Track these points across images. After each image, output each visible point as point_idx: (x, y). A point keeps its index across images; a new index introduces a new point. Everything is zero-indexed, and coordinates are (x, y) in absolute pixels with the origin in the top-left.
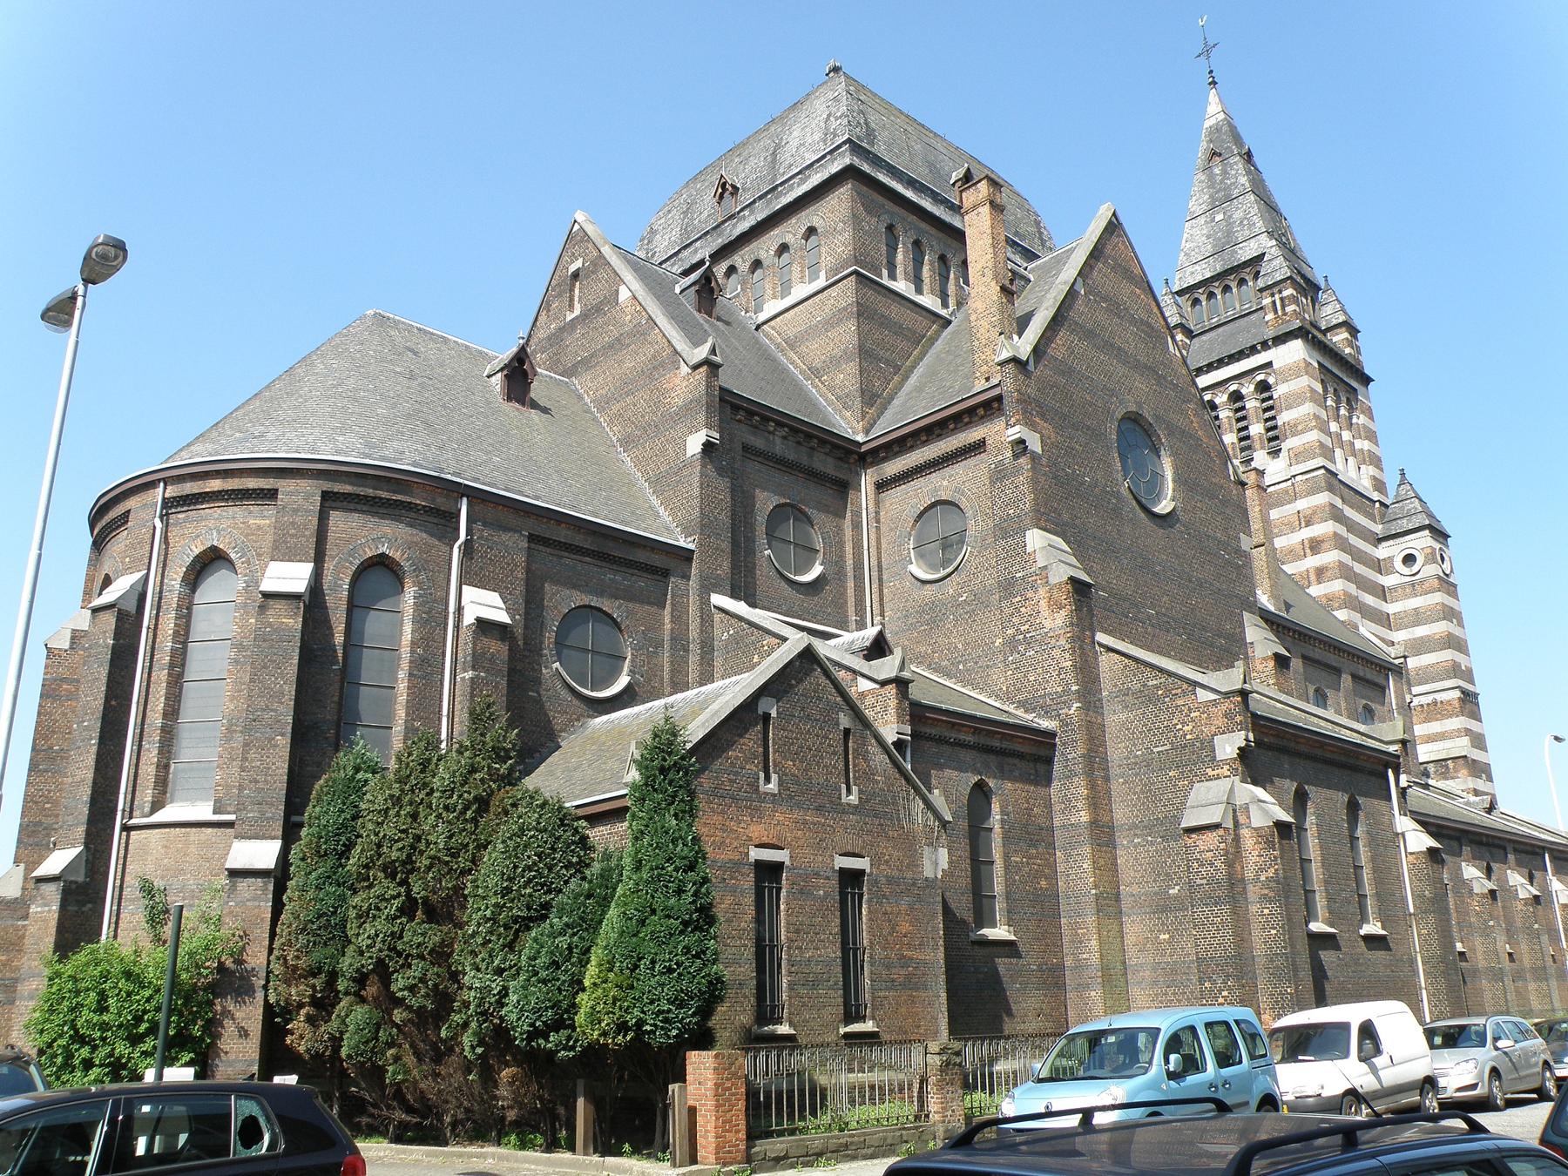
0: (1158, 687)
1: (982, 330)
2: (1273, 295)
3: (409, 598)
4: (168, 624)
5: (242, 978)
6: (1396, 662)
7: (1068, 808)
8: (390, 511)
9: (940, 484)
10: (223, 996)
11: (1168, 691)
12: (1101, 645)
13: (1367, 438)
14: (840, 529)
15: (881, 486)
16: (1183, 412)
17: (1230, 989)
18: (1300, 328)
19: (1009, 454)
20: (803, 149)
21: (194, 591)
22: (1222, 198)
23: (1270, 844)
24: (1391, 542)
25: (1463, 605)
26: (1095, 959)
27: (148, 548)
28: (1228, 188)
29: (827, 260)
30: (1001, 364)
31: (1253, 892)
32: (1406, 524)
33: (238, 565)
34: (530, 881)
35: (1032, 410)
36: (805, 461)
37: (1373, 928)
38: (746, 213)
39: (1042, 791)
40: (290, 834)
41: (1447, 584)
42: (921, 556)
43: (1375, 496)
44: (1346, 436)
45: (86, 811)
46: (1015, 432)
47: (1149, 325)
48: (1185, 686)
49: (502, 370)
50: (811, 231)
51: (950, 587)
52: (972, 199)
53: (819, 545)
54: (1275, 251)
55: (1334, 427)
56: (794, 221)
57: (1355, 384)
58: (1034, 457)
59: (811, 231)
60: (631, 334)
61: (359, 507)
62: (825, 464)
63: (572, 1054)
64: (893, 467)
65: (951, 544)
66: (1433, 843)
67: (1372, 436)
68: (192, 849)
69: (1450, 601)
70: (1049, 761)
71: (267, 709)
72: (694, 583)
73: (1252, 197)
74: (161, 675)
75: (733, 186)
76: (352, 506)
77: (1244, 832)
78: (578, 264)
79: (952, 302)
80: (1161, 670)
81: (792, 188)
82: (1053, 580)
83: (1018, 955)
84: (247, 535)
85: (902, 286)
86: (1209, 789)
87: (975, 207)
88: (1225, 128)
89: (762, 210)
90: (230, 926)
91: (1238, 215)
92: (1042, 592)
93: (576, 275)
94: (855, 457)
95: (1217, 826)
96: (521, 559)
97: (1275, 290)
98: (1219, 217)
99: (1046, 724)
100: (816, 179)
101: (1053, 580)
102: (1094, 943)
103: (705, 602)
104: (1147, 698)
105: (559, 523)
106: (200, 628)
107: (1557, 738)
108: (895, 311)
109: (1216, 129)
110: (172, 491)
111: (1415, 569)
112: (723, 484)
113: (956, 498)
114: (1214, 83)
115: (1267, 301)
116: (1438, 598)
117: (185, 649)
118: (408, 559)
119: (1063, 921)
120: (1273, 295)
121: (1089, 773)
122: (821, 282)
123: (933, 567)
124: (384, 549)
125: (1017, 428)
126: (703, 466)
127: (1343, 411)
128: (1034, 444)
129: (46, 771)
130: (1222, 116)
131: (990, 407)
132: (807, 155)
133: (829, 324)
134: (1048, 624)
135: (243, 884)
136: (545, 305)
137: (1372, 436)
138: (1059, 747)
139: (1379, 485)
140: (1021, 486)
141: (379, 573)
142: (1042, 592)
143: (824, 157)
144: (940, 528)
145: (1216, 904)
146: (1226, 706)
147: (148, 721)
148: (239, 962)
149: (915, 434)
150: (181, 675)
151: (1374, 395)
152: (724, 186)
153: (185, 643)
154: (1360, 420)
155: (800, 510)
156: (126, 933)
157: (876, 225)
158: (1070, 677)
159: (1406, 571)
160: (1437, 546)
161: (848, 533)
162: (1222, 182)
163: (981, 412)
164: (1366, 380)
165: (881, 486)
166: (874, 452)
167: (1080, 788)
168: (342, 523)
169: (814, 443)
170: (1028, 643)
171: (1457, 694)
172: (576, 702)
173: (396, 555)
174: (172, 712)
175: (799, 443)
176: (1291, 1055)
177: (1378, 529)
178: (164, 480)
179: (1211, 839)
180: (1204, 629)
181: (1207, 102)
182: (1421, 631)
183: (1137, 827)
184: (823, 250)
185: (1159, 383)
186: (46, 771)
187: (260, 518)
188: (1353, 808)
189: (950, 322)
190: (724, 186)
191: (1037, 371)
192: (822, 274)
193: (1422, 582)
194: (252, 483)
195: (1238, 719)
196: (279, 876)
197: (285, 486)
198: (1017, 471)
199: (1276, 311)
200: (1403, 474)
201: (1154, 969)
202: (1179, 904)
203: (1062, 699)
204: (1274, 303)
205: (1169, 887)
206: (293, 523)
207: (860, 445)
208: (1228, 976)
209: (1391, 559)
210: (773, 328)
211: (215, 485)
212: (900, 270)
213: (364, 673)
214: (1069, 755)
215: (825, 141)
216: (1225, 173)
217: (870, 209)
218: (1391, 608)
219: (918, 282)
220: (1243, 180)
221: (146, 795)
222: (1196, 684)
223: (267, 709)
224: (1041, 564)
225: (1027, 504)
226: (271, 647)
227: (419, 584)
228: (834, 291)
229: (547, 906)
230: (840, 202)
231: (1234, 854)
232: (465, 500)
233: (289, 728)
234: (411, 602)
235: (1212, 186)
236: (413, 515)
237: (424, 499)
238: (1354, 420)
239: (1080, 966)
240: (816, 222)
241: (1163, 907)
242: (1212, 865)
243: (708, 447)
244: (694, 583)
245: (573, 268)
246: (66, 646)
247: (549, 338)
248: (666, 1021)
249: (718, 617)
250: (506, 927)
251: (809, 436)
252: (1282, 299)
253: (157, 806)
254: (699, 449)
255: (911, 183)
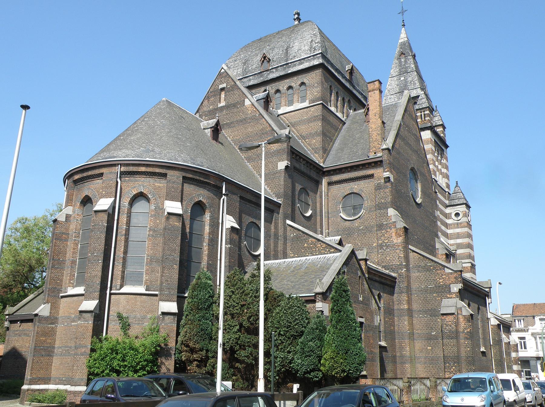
0: (431, 266)
1: (374, 135)
2: (421, 112)
3: (207, 216)
4: (124, 219)
5: (167, 351)
6: (453, 252)
7: (400, 303)
8: (203, 185)
9: (355, 187)
10: (161, 357)
11: (434, 268)
12: (410, 250)
13: (446, 168)
14: (315, 197)
15: (330, 184)
16: (423, 167)
17: (455, 366)
18: (430, 126)
19: (383, 181)
20: (300, 51)
21: (131, 207)
22: (403, 71)
23: (468, 321)
24: (451, 208)
25: (473, 233)
26: (408, 354)
27: (114, 189)
28: (406, 68)
29: (309, 96)
30: (383, 150)
31: (462, 336)
32: (457, 202)
33: (152, 200)
34: (297, 323)
35: (393, 167)
36: (308, 172)
37: (483, 349)
38: (274, 70)
39: (392, 297)
40: (180, 300)
41: (469, 225)
42: (344, 211)
43: (447, 190)
44: (440, 167)
45: (99, 287)
46: (387, 174)
47: (416, 135)
48: (441, 267)
49: (211, 128)
50: (303, 84)
51: (356, 224)
52: (372, 87)
53: (310, 203)
54: (423, 96)
55: (437, 163)
56: (295, 78)
57: (443, 148)
58: (392, 183)
59: (303, 84)
60: (251, 118)
61: (193, 183)
62: (313, 174)
63: (317, 379)
64: (336, 178)
65: (356, 209)
66: (499, 323)
67: (447, 168)
68: (138, 303)
69: (469, 231)
70: (394, 287)
71: (170, 255)
72: (281, 216)
73: (416, 73)
74: (121, 238)
75: (269, 59)
76: (191, 182)
77: (460, 316)
78: (224, 85)
79: (345, 115)
80: (432, 260)
81: (295, 65)
82: (398, 227)
83: (386, 351)
84: (155, 189)
85: (333, 109)
86: (449, 301)
87: (373, 90)
88: (407, 44)
89: (281, 71)
90: (163, 333)
91: (410, 79)
92: (393, 230)
93: (223, 89)
94: (322, 172)
95: (453, 314)
96: (238, 204)
97: (422, 111)
98: (402, 79)
99: (393, 274)
100: (306, 65)
101: (398, 227)
102: (408, 348)
103: (285, 222)
104: (427, 269)
105: (248, 192)
106: (134, 221)
107: (500, 283)
108: (331, 119)
109: (403, 44)
110: (123, 169)
111: (459, 218)
112: (290, 181)
113: (360, 193)
114: (404, 25)
115: (419, 114)
116: (466, 229)
117: (129, 228)
118: (208, 203)
119: (396, 341)
120: (421, 112)
121: (407, 292)
122: (306, 104)
123: (349, 215)
124: (201, 199)
125: (388, 173)
126: (285, 174)
127: (439, 158)
128: (392, 179)
129: (58, 268)
130: (406, 39)
131: (378, 164)
132: (302, 54)
133: (310, 121)
134: (395, 241)
135: (84, 314)
136: (207, 97)
137: (447, 168)
138: (397, 283)
139: (448, 186)
140: (387, 194)
141: (199, 208)
142: (393, 230)
143: (310, 57)
144: (353, 202)
145: (452, 339)
146: (455, 275)
147: (117, 254)
148: (166, 345)
149: (346, 168)
150: (128, 238)
151: (449, 152)
152: (265, 58)
153: (129, 226)
154: (444, 161)
155: (307, 192)
156: (113, 332)
157: (326, 85)
158: (403, 260)
159: (456, 219)
160: (467, 211)
161: (318, 199)
162: (404, 65)
163: (373, 164)
164: (447, 147)
165: (330, 184)
166: (329, 172)
167: (404, 297)
168: (189, 188)
169: (312, 167)
170: (387, 246)
171: (470, 265)
172: (250, 256)
173: (204, 201)
174: (125, 252)
175: (307, 166)
176: (453, 390)
177: (447, 202)
178: (121, 164)
179: (451, 318)
180: (427, 243)
181: (400, 33)
182: (459, 241)
183: (421, 311)
184: (308, 92)
185: (418, 157)
186: (58, 268)
187: (160, 183)
188: (479, 309)
189: (345, 123)
190: (265, 58)
191: (393, 153)
192: (308, 101)
193: (461, 223)
194: (157, 170)
195: (459, 280)
196: (179, 315)
197: (170, 173)
198: (386, 187)
199: (422, 119)
200: (457, 183)
201: (425, 358)
202: (435, 338)
203: (400, 267)
204: (421, 115)
205: (432, 332)
206: (173, 187)
207: (323, 168)
208: (455, 362)
209: (451, 213)
210: (285, 117)
211: (143, 169)
212: (332, 103)
213: (193, 243)
214: (401, 285)
215: (310, 51)
216: (406, 61)
217: (326, 80)
218: (449, 231)
219: (337, 107)
220: (413, 66)
221: (119, 282)
222: (445, 266)
223: (170, 255)
224: (393, 220)
225: (389, 199)
226: (171, 233)
227: (211, 212)
228: (312, 109)
229: (302, 332)
230: (317, 75)
231: (457, 324)
232: (224, 183)
233: (178, 262)
234: (208, 218)
235: (400, 65)
236: (209, 187)
237: (213, 182)
238: (442, 161)
239: (402, 356)
240: (305, 81)
241: (429, 338)
242: (451, 326)
243: (287, 167)
244: (281, 216)
245: (221, 86)
246: (64, 220)
247: (209, 111)
248: (357, 370)
249: (289, 228)
250: (289, 338)
251: (311, 164)
252: (424, 114)
253: (122, 286)
254: (284, 168)
255: (337, 70)
